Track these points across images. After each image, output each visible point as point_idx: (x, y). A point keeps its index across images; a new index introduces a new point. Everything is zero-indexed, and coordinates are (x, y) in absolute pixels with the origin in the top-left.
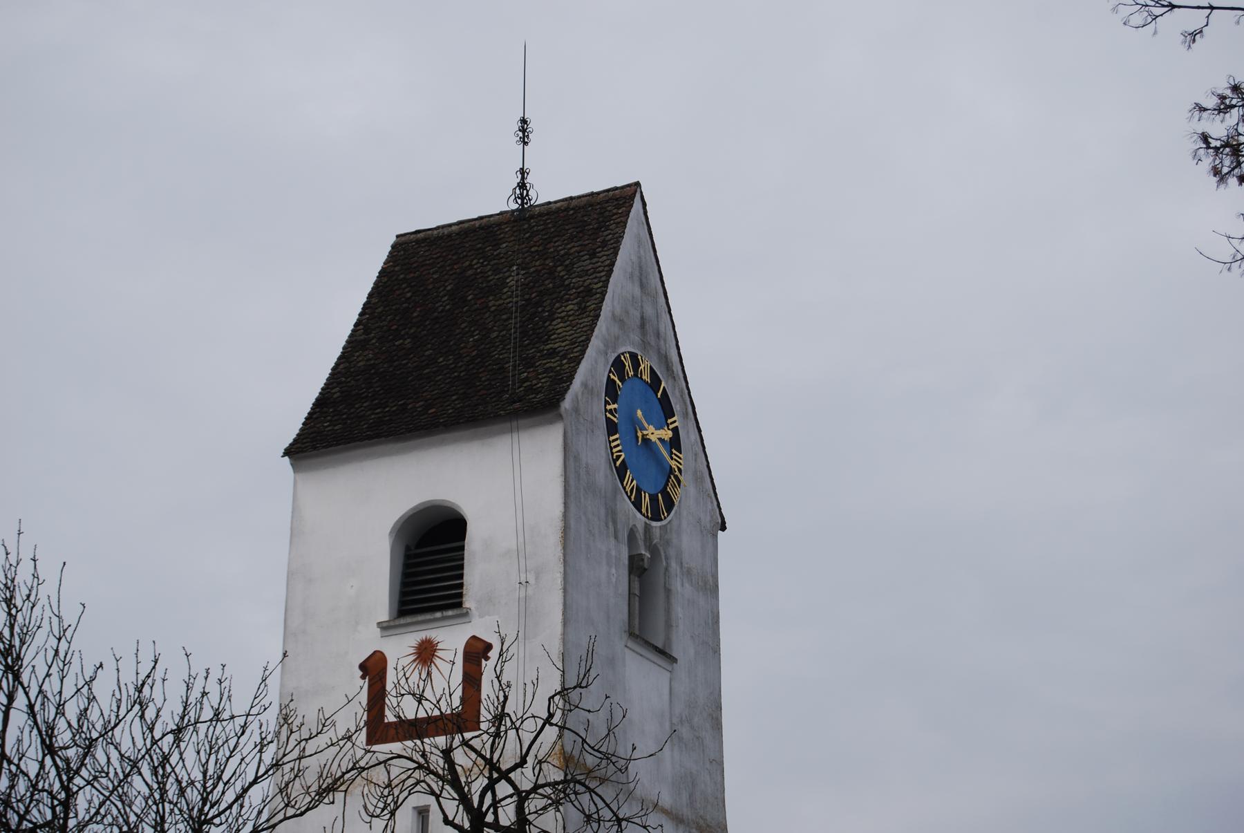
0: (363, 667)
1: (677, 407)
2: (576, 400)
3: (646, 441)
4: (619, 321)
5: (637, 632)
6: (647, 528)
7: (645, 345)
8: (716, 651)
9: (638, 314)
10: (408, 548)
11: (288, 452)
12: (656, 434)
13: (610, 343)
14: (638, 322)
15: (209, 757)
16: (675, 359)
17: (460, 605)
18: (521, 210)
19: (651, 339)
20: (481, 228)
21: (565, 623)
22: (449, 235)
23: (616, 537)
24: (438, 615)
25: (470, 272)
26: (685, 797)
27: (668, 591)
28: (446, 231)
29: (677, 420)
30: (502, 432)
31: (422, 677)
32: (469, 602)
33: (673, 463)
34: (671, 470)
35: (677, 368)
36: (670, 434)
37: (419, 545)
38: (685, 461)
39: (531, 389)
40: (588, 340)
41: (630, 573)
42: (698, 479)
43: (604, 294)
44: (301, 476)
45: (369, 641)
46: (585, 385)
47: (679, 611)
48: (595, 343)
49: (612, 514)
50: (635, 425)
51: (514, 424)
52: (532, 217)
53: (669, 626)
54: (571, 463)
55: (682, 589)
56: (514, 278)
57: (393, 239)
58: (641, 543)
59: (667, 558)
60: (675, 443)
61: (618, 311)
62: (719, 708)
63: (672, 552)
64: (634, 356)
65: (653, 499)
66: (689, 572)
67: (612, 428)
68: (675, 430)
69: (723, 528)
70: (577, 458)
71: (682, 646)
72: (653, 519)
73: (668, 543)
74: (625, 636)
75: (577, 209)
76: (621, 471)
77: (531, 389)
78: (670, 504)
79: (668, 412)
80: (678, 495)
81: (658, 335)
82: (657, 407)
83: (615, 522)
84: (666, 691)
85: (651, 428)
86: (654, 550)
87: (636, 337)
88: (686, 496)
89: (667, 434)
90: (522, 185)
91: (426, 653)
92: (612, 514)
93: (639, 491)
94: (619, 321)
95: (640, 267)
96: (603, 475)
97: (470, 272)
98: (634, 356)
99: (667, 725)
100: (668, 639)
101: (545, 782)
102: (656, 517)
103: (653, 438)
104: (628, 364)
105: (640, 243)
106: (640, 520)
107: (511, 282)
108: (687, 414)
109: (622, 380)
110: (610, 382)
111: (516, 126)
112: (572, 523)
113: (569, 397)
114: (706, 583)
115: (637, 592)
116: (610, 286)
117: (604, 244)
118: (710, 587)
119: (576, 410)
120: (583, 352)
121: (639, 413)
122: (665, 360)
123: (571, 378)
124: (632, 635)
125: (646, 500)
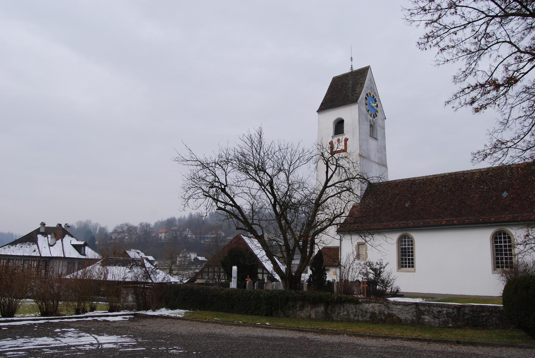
0: (329, 143)
1: (377, 100)
2: (360, 100)
3: (372, 106)
4: (367, 87)
5: (372, 136)
6: (373, 120)
7: (372, 91)
8: (385, 138)
9: (370, 86)
10: (336, 125)
11: (317, 112)
12: (373, 105)
13: (366, 91)
14: (370, 87)
15: (290, 167)
16: (377, 93)
17: (343, 133)
18: (352, 71)
19: (373, 90)
20: (346, 75)
21: (359, 135)
22: (341, 76)
23: (367, 121)
24: (340, 135)
25: (344, 82)
26: (380, 160)
27: (376, 129)
28: (340, 76)
29: (377, 103)
30: (349, 106)
31: (284, 176)
32: (345, 132)
33: (377, 109)
34: (377, 110)
35: (377, 94)
36: (376, 105)
37: (338, 124)
38: (379, 109)
39: (353, 99)
40: (362, 91)
41: (370, 127)
42: (381, 112)
43: (364, 84)
44: (320, 115)
45: (330, 139)
46: (362, 98)
47: (378, 132)
48: (363, 91)
49: (367, 118)
50: (370, 104)
51: (351, 105)
52: (353, 72)
53: (377, 134)
54: (360, 110)
55: (379, 129)
56: (351, 82)
57: (332, 78)
58: (372, 122)
59: (376, 124)
60: (377, 106)
61: (367, 86)
62: (385, 147)
63: (377, 123)
64: (370, 93)
65: (374, 115)
66: (380, 126)
67: (366, 104)
68: (377, 104)
69: (386, 119)
70: (361, 109)
71: (379, 137)
72: (374, 118)
73: (376, 122)
74: (369, 136)
75: (360, 71)
76: (368, 111)
77: (353, 99)
78: (376, 116)
79: (376, 101)
80: (378, 114)
81: (374, 89)
82: (374, 101)
83: (367, 119)
84: (376, 145)
85: (373, 104)
86: (374, 123)
87: (370, 90)
88: (379, 114)
89: (376, 105)
90: (352, 68)
91: (339, 140)
92: (367, 118)
93: (371, 114)
94: (367, 87)
95: (371, 79)
96: (365, 112)
97: (344, 82)
98: (370, 93)
99: (377, 150)
100: (377, 136)
101: (266, 256)
102: (374, 118)
103: (373, 106)
104: (369, 94)
105: (370, 75)
106: (371, 118)
107: (350, 83)
108: (379, 102)
109: (368, 97)
110: (366, 97)
111: (353, 60)
112: (360, 119)
113: (359, 100)
114: (383, 127)
115: (371, 129)
116: (365, 82)
117: (364, 76)
118: (384, 128)
119: (360, 102)
120: (361, 93)
121: (371, 102)
122: (375, 93)
123: (359, 97)
124: (370, 136)
125: (372, 115)
